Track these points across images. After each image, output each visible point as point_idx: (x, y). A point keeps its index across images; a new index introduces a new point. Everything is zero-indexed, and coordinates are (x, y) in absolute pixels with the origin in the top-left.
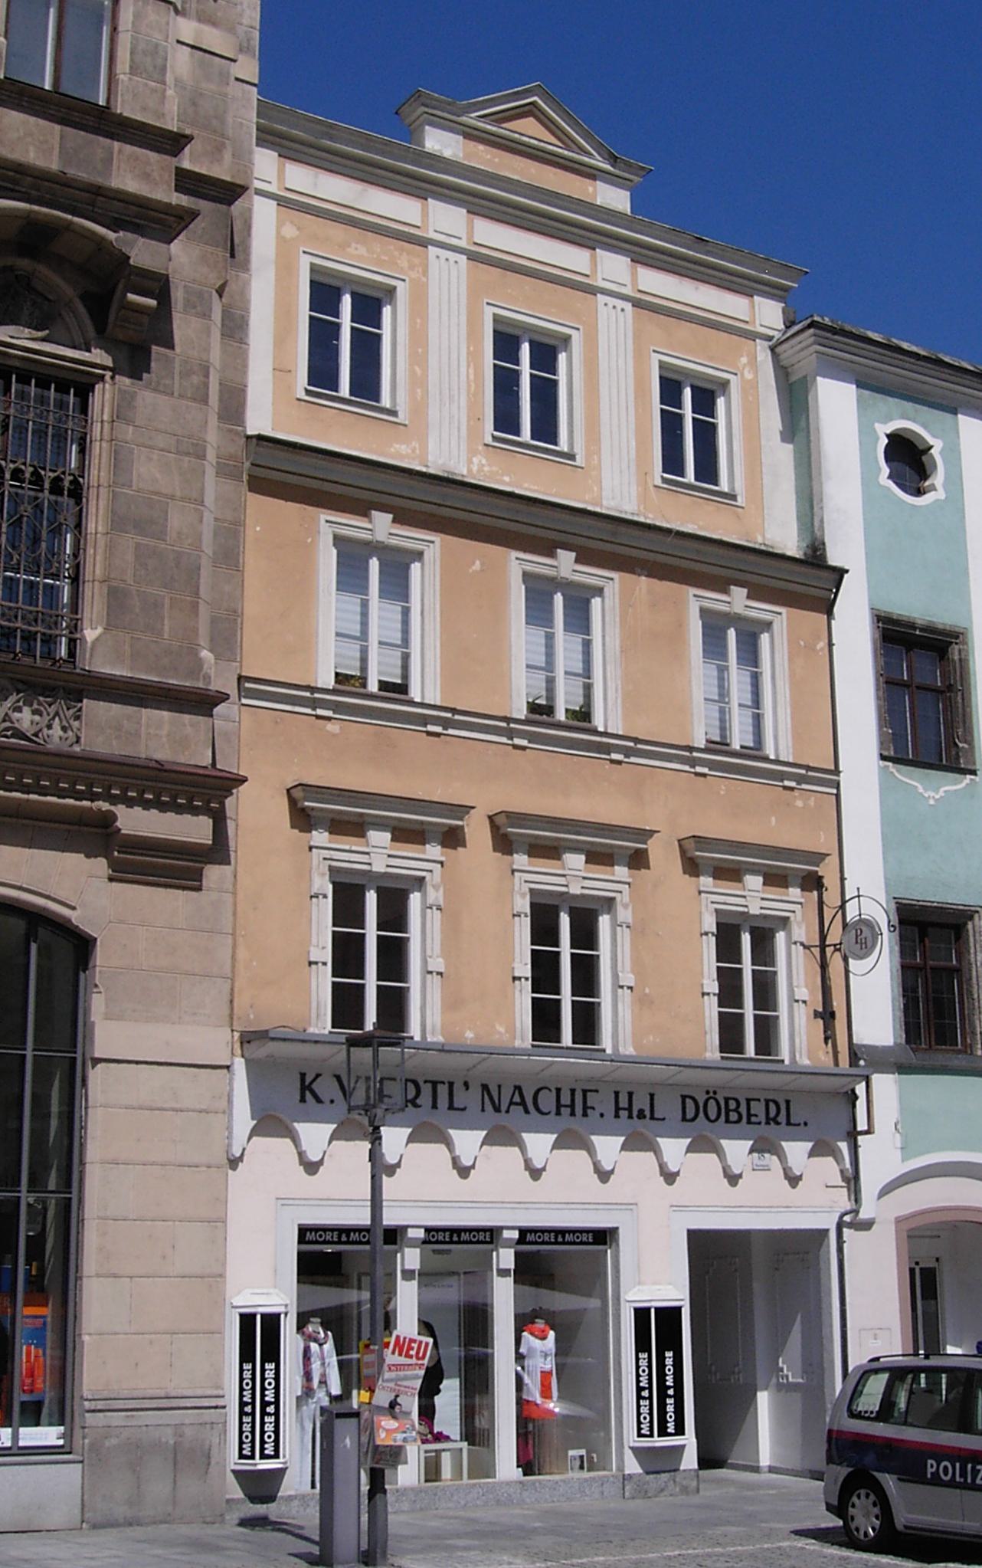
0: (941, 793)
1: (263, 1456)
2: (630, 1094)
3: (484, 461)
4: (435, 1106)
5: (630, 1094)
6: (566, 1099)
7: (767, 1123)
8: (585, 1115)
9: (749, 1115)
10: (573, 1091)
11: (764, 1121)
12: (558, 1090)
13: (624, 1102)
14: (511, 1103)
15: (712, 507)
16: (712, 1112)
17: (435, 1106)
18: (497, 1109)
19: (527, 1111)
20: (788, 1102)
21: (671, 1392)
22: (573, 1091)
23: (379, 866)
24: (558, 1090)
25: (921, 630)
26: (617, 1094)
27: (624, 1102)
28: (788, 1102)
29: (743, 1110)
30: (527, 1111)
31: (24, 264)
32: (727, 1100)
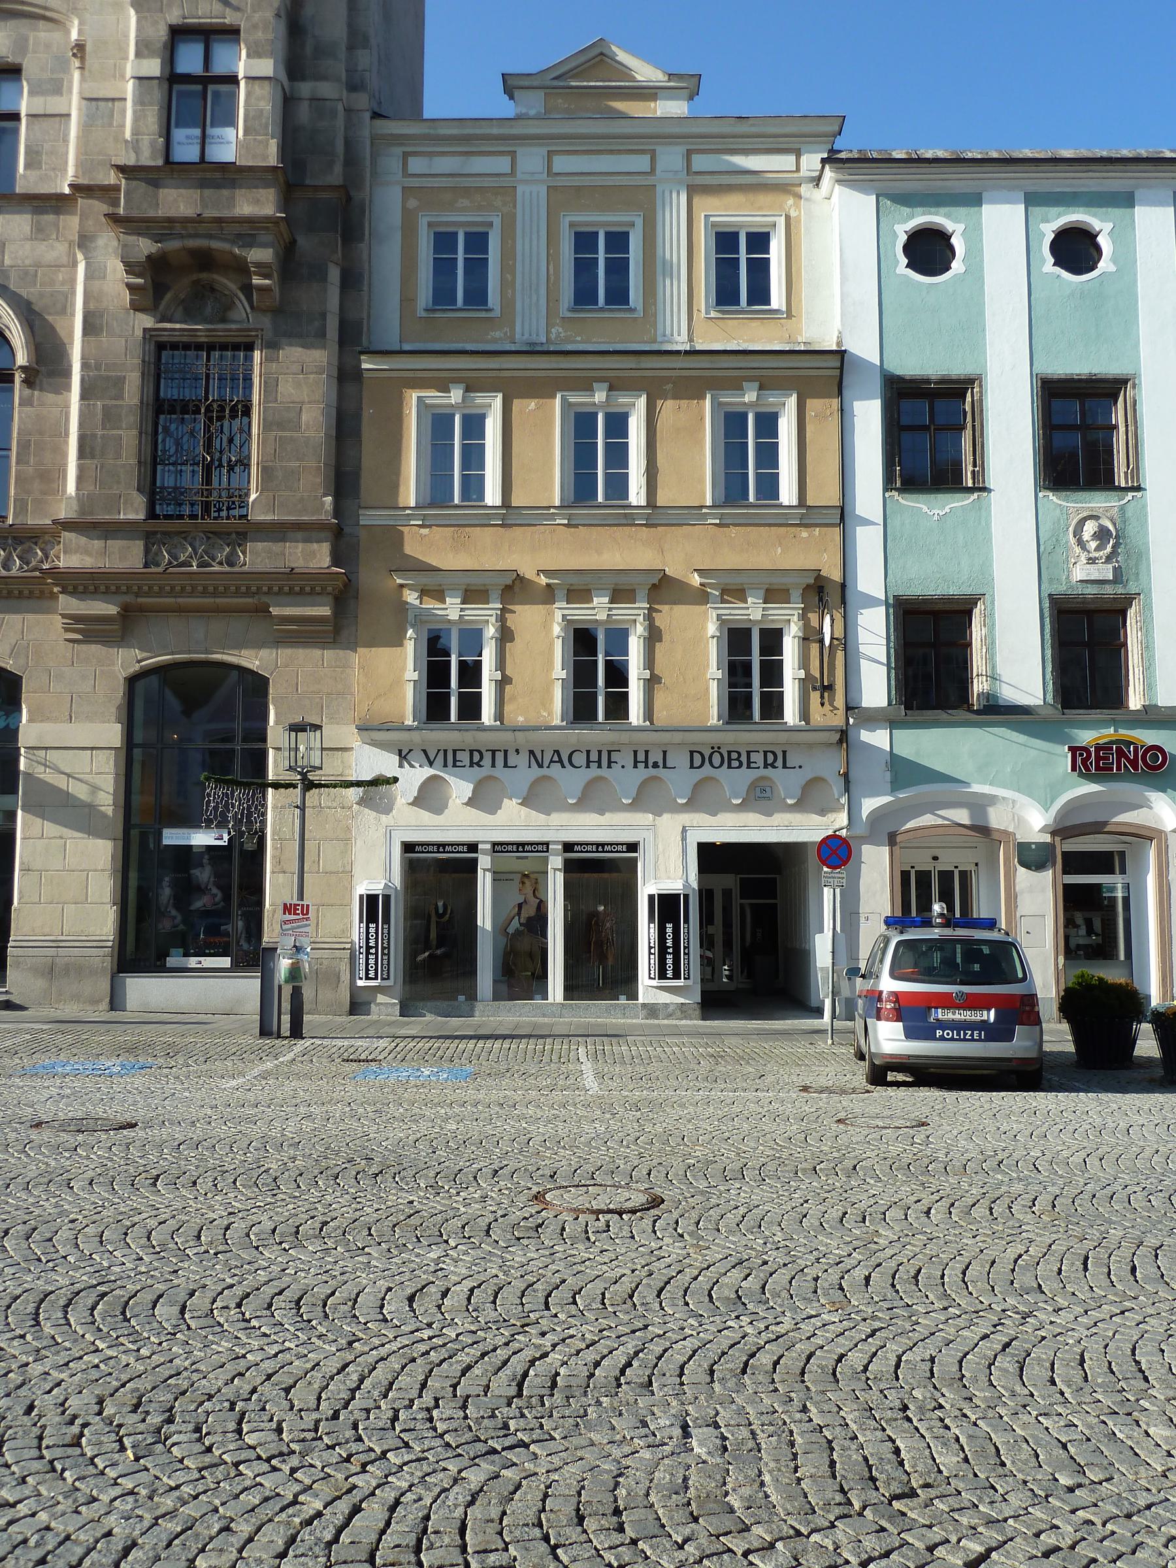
0: (947, 510)
1: (367, 978)
2: (647, 752)
3: (561, 330)
4: (493, 765)
5: (647, 752)
6: (594, 756)
7: (471, 766)
8: (609, 767)
9: (749, 762)
10: (600, 752)
11: (762, 765)
12: (588, 752)
13: (641, 757)
14: (551, 761)
15: (755, 324)
16: (717, 759)
17: (493, 765)
18: (540, 766)
19: (563, 766)
20: (784, 752)
21: (670, 950)
22: (600, 752)
23: (602, 616)
24: (588, 752)
25: (935, 383)
26: (635, 752)
27: (641, 757)
28: (784, 752)
29: (744, 759)
30: (563, 766)
31: (334, 274)
32: (729, 753)
